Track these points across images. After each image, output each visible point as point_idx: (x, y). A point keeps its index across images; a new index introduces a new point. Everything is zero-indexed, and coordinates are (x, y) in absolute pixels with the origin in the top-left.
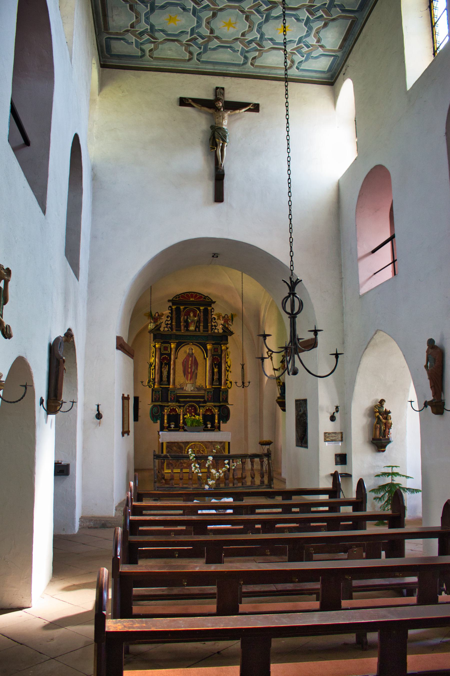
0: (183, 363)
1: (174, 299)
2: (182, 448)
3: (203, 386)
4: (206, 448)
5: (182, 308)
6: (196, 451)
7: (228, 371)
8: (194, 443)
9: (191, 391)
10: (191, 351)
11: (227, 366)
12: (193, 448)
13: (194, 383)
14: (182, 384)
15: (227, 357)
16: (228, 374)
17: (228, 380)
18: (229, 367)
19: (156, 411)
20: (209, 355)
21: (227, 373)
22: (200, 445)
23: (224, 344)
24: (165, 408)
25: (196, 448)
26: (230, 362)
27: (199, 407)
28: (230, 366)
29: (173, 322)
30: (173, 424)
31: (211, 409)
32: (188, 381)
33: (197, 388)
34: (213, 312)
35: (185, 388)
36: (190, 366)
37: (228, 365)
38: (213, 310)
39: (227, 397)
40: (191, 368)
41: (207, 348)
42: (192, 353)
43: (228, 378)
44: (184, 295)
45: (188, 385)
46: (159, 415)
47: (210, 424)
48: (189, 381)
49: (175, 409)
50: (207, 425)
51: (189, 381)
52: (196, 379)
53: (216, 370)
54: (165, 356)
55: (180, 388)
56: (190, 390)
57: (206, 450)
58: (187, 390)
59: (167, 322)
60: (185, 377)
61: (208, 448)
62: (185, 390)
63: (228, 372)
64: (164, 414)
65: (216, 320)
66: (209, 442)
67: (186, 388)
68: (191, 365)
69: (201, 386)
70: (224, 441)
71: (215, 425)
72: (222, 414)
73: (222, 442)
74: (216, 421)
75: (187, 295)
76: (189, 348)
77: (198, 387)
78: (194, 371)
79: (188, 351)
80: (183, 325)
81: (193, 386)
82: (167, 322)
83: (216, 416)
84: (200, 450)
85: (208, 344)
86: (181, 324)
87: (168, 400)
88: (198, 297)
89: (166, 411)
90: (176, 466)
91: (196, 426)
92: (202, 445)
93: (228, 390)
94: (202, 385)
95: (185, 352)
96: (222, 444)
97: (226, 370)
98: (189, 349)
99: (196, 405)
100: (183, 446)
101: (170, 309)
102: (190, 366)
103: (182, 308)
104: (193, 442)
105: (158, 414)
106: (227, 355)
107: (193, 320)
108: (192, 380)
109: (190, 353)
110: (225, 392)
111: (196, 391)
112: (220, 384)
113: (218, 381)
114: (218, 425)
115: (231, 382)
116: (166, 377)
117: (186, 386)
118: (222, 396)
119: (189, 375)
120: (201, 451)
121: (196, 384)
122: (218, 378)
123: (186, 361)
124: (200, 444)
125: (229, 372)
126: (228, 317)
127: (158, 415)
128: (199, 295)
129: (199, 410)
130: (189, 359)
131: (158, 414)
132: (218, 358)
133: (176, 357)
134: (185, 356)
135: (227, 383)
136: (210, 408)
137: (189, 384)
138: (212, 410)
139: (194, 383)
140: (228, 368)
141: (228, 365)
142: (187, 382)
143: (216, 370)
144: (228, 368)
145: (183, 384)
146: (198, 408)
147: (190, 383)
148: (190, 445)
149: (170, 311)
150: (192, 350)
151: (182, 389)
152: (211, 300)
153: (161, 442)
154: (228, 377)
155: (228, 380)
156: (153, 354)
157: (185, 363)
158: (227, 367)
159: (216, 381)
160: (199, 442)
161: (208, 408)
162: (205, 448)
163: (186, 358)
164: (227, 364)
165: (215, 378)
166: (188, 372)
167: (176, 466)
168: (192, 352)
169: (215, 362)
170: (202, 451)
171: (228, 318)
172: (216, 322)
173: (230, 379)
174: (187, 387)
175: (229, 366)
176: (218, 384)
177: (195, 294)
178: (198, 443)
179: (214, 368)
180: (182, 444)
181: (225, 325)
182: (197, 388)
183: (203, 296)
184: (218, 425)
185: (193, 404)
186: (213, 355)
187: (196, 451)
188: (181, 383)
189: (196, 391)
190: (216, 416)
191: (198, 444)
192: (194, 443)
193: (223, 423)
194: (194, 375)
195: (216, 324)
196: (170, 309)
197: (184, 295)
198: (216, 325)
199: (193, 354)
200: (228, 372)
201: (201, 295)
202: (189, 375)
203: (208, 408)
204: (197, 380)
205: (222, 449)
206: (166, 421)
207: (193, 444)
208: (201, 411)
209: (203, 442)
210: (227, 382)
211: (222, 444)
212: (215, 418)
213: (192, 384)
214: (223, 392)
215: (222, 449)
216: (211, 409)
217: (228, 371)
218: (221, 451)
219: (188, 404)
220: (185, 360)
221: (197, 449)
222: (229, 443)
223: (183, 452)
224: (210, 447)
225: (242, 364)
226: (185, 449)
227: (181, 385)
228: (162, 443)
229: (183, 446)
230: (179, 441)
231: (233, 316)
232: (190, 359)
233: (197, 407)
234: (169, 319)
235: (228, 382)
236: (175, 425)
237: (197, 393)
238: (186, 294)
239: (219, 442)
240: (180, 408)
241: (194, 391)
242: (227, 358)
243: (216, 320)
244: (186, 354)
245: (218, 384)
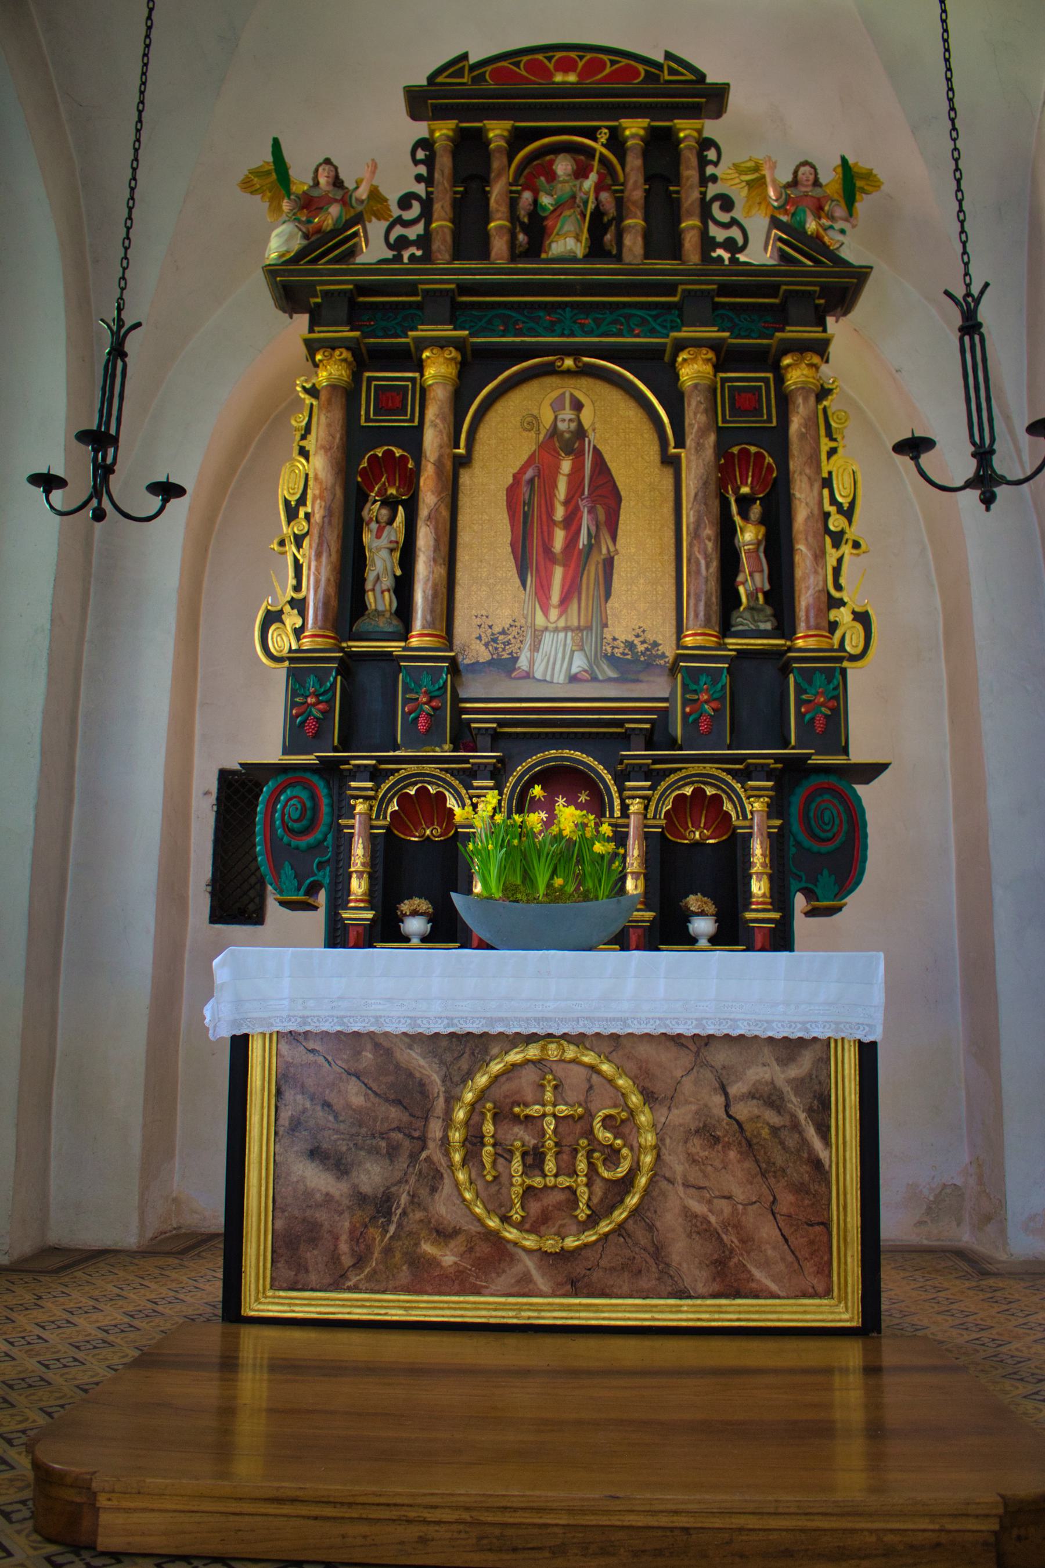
0: (512, 491)
1: (440, 79)
2: (422, 1084)
3: (655, 644)
4: (649, 1097)
5: (497, 131)
6: (550, 1125)
7: (838, 538)
8: (533, 1052)
9: (573, 679)
10: (568, 414)
11: (828, 507)
12: (529, 1095)
13: (589, 628)
14: (503, 632)
15: (825, 445)
16: (840, 560)
17: (841, 603)
18: (848, 513)
19: (295, 815)
20: (695, 417)
21: (832, 556)
22: (593, 1068)
23: (801, 348)
24: (353, 784)
25: (549, 1096)
26: (848, 481)
27: (620, 778)
28: (852, 504)
29: (435, 216)
30: (415, 913)
31: (717, 800)
32: (546, 613)
33: (612, 660)
34: (716, 164)
35: (523, 663)
36: (560, 513)
37: (833, 501)
38: (711, 154)
39: (835, 711)
40: (571, 522)
41: (677, 377)
42: (573, 426)
43: (838, 587)
44: (517, 64)
45: (547, 637)
46: (320, 843)
47: (711, 908)
48: (554, 613)
49: (441, 798)
50: (686, 916)
51: (554, 613)
52: (608, 595)
53: (748, 535)
54: (389, 454)
55: (490, 663)
56: (560, 677)
57: (643, 1119)
58: (538, 675)
59: (398, 231)
60: (524, 584)
61: (671, 1100)
62: (528, 676)
63: (836, 545)
64: (352, 835)
65: (737, 213)
66: (677, 1040)
67: (532, 662)
68: (566, 503)
69: (641, 648)
70: (820, 1032)
71: (749, 915)
72: (807, 843)
73: (801, 1043)
74: (758, 887)
75: (535, 67)
76: (555, 394)
77: (618, 652)
78: (590, 547)
79: (547, 417)
80: (501, 227)
81: (582, 649)
82: (398, 231)
83: (758, 851)
84: (589, 1115)
85: (680, 346)
86: (492, 225)
87: (395, 739)
88: (608, 70)
89: (360, 807)
90: (360, 1261)
91: (554, 895)
92: (605, 1067)
93: (843, 672)
94: (650, 637)
95: (532, 423)
96: (805, 1063)
97: (827, 531)
98: (557, 405)
99: (594, 764)
100: (435, 1078)
101: (421, 154)
102: (560, 513)
103: (497, 131)
104: (532, 1038)
105: (311, 840)
106: (822, 432)
107: (573, 197)
108: (574, 606)
109: (562, 426)
110: (819, 679)
111: (610, 680)
112: (785, 626)
113: (769, 611)
114: (776, 915)
115: (862, 618)
116: (387, 582)
117: (535, 647)
118: (799, 703)
119: (558, 572)
120: (597, 1125)
121: (608, 635)
122: (766, 594)
123: (531, 481)
124: (588, 1058)
125: (846, 549)
126: (816, 183)
127: (311, 848)
128: (613, 63)
129: (617, 802)
130: (558, 467)
131: (311, 840)
132: (758, 455)
133: (462, 451)
134: (524, 447)
135: (833, 626)
136: (710, 791)
137: (556, 630)
138: (728, 806)
139: (589, 628)
140: (836, 522)
141: (833, 501)
142: (540, 620)
143: (748, 535)
144: (836, 522)
145: (514, 632)
146: (614, 789)
147: (561, 623)
148: (496, 1067)
149: (422, 170)
150: (578, 406)
151: (506, 665)
152: (690, 77)
153: (225, 1032)
154: (842, 581)
155: (841, 603)
156: (303, 437)
157: (525, 490)
158: (827, 515)
159: (750, 608)
160: (579, 1040)
161: (688, 791)
162: (635, 1099)
163: (532, 457)
164: (826, 492)
165: (741, 589)
166: (547, 550)
167: (360, 1261)
168: (580, 424)
169: (745, 490)
170: (608, 1122)
171: (817, 192)
172: (734, 222)
173: (854, 596)
174: (538, 657)
175: (846, 506)
176: (767, 626)
177: (589, 56)
178: (571, 1052)
179: (737, 519)
180: (418, 1061)
181: (802, 224)
182: (612, 660)
183: (641, 68)
184: (776, 915)
185: (577, 755)
186: (724, 437)
187: (550, 1125)
188: (497, 629)
189: (610, 680)
190: (758, 851)
191: (574, 1061)
192: (533, 1052)
193: (810, 913)
194: (593, 571)
195: (735, 233)
196: (421, 154)
197: (517, 64)
198: (740, 242)
199: (580, 433)
200: (836, 545)
201: (624, 62)
202: (558, 572)
203: (688, 791)
204: (613, 603)
205: (802, 1116)
206: (358, 886)
207: (527, 1062)
208: (635, 806)
209: (615, 1037)
210: (833, 615)
211: (805, 1063)
212: (749, 865)
213: (579, 629)
214: (807, 675)
215: (802, 1116)
216: (717, 800)
217: (838, 538)
218: (796, 1126)
219: (531, 761)
220: (530, 473)
221: (563, 1110)
222: (868, 1052)
223: (435, 1129)
224: (688, 1086)
225: (959, 293)
226: (452, 1099)
227: (495, 640)
228: (240, 1044)
229: (435, 1078)
230: (388, 1028)
231: (859, 184)
232: (566, 466)
233: (608, 778)
234: (416, 209)
235: (843, 616)
236: (431, 919)
237: (612, 691)
238: (525, 59)
239: (771, 1039)
240: (468, 787)
241: (594, 679)
242: (824, 456)
243: (737, 213)
244: (533, 434)
245: (767, 626)
